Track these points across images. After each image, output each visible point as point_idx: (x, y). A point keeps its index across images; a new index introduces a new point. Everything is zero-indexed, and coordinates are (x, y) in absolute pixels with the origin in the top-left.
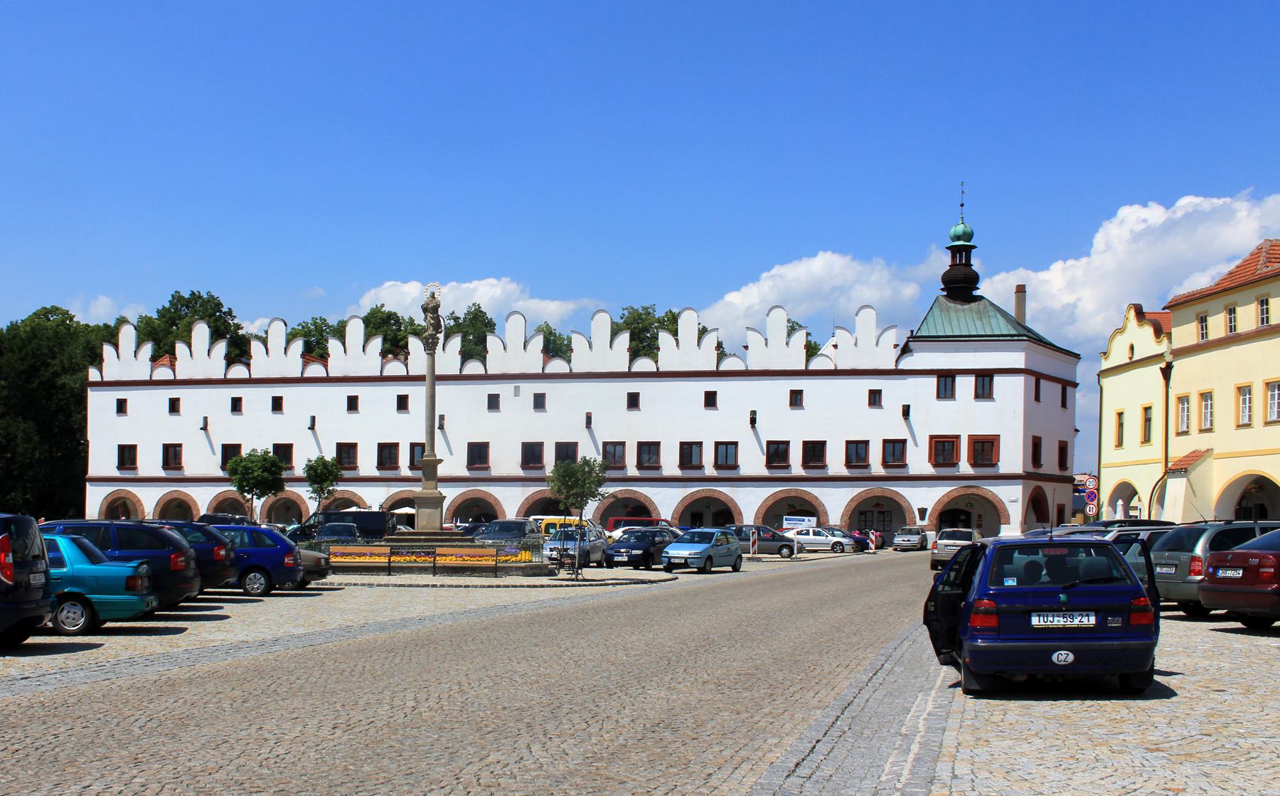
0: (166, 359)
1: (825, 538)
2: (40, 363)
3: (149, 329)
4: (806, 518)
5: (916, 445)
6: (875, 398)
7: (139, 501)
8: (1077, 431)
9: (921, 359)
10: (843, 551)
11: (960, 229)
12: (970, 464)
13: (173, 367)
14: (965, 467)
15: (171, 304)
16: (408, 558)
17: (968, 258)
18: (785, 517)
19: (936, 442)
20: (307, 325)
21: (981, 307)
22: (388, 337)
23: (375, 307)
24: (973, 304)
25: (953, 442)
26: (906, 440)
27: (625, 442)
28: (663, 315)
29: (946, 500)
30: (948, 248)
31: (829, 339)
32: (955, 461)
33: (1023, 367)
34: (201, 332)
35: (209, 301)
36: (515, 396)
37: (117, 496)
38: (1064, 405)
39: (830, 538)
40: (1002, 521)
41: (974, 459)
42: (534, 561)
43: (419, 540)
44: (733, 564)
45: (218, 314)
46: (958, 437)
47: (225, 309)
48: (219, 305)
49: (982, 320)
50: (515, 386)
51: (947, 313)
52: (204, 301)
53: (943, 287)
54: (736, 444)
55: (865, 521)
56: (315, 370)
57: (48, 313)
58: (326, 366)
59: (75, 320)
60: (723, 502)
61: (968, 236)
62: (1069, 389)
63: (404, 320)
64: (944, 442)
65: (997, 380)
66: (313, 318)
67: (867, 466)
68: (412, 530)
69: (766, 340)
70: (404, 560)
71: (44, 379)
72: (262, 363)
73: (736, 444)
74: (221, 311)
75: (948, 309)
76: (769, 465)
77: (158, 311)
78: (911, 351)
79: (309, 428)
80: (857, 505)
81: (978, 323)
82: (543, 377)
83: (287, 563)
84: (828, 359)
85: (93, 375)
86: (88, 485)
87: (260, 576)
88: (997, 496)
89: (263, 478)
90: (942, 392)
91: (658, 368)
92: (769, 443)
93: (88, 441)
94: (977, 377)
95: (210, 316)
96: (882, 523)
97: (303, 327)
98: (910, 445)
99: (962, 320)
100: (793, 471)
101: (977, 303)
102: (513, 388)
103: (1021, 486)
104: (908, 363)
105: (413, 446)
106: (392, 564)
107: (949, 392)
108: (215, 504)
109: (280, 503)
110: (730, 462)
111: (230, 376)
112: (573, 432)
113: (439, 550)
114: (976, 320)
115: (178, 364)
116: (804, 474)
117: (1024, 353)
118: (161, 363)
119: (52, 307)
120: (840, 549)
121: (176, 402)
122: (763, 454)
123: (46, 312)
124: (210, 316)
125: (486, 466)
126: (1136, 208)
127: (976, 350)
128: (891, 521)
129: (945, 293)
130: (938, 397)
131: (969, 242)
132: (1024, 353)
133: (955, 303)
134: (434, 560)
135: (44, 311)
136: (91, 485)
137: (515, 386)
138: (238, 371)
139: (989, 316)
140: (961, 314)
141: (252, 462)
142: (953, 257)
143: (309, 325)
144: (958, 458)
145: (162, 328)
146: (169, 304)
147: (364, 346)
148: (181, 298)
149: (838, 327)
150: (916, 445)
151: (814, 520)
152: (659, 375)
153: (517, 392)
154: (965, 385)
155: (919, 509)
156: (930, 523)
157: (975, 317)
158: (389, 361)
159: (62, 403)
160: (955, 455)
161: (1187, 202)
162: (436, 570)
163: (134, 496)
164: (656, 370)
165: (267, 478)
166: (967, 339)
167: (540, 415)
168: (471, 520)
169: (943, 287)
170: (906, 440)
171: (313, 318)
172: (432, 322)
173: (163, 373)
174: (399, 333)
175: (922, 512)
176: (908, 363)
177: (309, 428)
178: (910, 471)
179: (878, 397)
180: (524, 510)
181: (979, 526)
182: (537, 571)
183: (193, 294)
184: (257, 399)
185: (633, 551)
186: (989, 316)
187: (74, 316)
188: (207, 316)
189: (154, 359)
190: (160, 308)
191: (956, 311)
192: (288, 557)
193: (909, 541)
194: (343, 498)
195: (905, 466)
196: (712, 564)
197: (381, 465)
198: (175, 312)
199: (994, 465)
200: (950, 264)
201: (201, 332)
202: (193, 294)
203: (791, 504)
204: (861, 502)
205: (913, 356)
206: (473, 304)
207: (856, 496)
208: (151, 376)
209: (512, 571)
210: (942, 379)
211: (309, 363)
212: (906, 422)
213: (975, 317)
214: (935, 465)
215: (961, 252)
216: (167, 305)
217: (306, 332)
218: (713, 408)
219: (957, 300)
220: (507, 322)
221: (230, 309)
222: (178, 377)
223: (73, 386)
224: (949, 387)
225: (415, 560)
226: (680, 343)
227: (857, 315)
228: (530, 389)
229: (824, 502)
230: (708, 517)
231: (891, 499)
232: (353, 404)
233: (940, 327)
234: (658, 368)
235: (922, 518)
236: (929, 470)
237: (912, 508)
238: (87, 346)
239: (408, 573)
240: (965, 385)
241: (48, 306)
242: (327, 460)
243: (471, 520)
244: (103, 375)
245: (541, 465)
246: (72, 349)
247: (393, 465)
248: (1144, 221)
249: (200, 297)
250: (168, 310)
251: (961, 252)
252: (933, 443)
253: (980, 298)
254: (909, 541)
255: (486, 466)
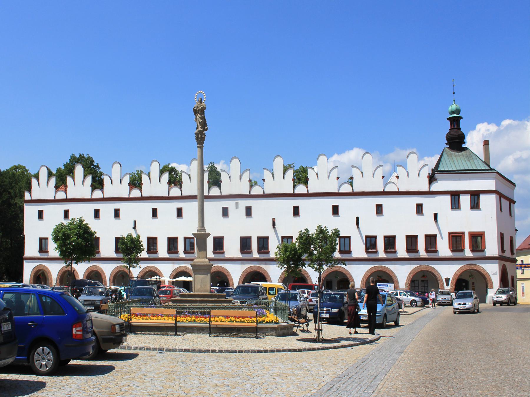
0: (63, 188)
1: (406, 297)
2: (2, 190)
3: (59, 173)
4: (389, 284)
5: (442, 238)
6: (419, 208)
7: (49, 272)
8: (516, 230)
9: (440, 185)
10: (416, 306)
11: (454, 107)
12: (470, 250)
13: (65, 191)
14: (468, 253)
15: (70, 161)
16: (189, 319)
17: (458, 124)
18: (378, 283)
19: (452, 236)
20: (134, 175)
21: (468, 154)
22: (172, 181)
23: (165, 165)
24: (463, 152)
25: (461, 236)
26: (436, 235)
27: (293, 237)
28: (299, 168)
29: (459, 273)
30: (448, 119)
31: (393, 173)
32: (462, 248)
33: (494, 189)
34: (79, 170)
35: (88, 159)
36: (236, 208)
37: (38, 269)
38: (510, 214)
39: (409, 297)
40: (489, 286)
41: (472, 247)
42: (280, 322)
43: (196, 302)
44: (395, 320)
45: (92, 166)
46: (463, 233)
47: (95, 164)
48: (92, 161)
49: (470, 161)
50: (236, 202)
51: (451, 157)
52: (85, 159)
53: (447, 142)
54: (349, 238)
55: (415, 286)
56: (136, 193)
57: (16, 168)
58: (141, 191)
59: (29, 172)
60: (344, 274)
61: (458, 111)
62: (512, 204)
63: (179, 172)
64: (456, 236)
65: (482, 197)
66: (137, 171)
67: (417, 252)
68: (188, 293)
69: (362, 173)
70: (187, 320)
71: (4, 199)
72: (110, 191)
73: (349, 238)
74: (93, 165)
75: (451, 155)
76: (367, 251)
77: (64, 165)
78: (436, 180)
79: (133, 228)
80: (413, 276)
81: (468, 163)
82: (250, 196)
83: (76, 335)
84: (394, 185)
85: (27, 196)
86: (24, 261)
87: (48, 350)
88: (485, 271)
89: (77, 243)
90: (453, 205)
91: (308, 191)
92: (367, 237)
93: (24, 236)
94: (471, 195)
95: (88, 168)
96: (423, 287)
97: (132, 175)
98: (439, 238)
99: (460, 161)
100: (379, 255)
101: (465, 152)
102: (235, 203)
103: (498, 264)
104: (435, 187)
105: (185, 238)
106: (178, 324)
107: (457, 205)
108: (87, 274)
109: (119, 273)
110: (347, 249)
111: (93, 197)
112: (267, 231)
113: (213, 312)
114: (466, 161)
115: (68, 189)
116: (385, 256)
117: (494, 181)
118: (61, 189)
119: (18, 165)
120: (415, 304)
121: (68, 212)
122: (364, 244)
123: (16, 168)
124: (88, 168)
125: (222, 251)
126: (485, 124)
127: (470, 179)
128: (428, 286)
129: (448, 146)
130: (452, 208)
131: (459, 115)
132: (494, 181)
133: (454, 152)
134: (210, 321)
135: (14, 167)
136: (26, 262)
137: (236, 202)
138: (98, 194)
139: (473, 159)
140: (458, 158)
141: (71, 229)
142: (451, 124)
143: (135, 174)
144: (464, 246)
145: (64, 173)
146: (69, 161)
147: (160, 178)
148: (75, 158)
149: (398, 165)
150: (442, 238)
151: (392, 285)
152: (309, 195)
153: (237, 207)
154: (465, 200)
155: (445, 279)
156: (451, 288)
157: (466, 159)
158: (172, 188)
159: (13, 213)
160: (462, 245)
161: (506, 122)
162: (213, 330)
163: (47, 268)
164: (307, 192)
165: (81, 244)
166: (465, 172)
167: (249, 220)
168: (218, 284)
169: (447, 142)
170: (436, 235)
171: (137, 171)
172: (201, 121)
173: (61, 195)
174: (176, 179)
175: (447, 280)
176: (435, 187)
177: (133, 228)
178: (439, 254)
179: (420, 209)
180: (242, 279)
181: (473, 289)
182: (285, 331)
183: (80, 155)
184: (108, 209)
185: (333, 310)
186: (473, 159)
187: (28, 170)
188: (87, 167)
189: (57, 187)
190: (65, 163)
191: (456, 156)
192: (76, 327)
193: (445, 299)
194: (151, 271)
195: (436, 251)
196: (386, 320)
197: (170, 251)
198: (72, 165)
199: (483, 251)
200: (450, 128)
201: (79, 170)
202: (80, 155)
203: (379, 275)
204: (416, 274)
205: (437, 183)
206: (211, 163)
207: (412, 270)
208: (55, 197)
209: (267, 331)
210: (453, 197)
211: (133, 188)
212: (436, 223)
213: (466, 159)
214: (453, 251)
215: (455, 121)
216: (68, 162)
217: (133, 178)
218: (337, 215)
219: (455, 150)
220: (231, 163)
221: (97, 164)
222: (69, 197)
223: (21, 204)
224: (457, 202)
225: (195, 321)
226: (319, 175)
227: (407, 157)
228: (244, 203)
229: (397, 275)
230: (335, 285)
231: (431, 272)
232: (154, 213)
233: (449, 165)
234: (308, 191)
235: (447, 285)
236: (448, 253)
237: (442, 278)
238: (28, 182)
239: (190, 332)
240: (465, 200)
241: (17, 165)
242: (134, 237)
243: (218, 284)
244: (32, 196)
245: (250, 251)
246: (21, 184)
247: (175, 251)
248: (488, 130)
249: (84, 157)
250: (69, 164)
251: (455, 121)
252: (451, 237)
253: (466, 149)
254: (445, 299)
255: (222, 251)
